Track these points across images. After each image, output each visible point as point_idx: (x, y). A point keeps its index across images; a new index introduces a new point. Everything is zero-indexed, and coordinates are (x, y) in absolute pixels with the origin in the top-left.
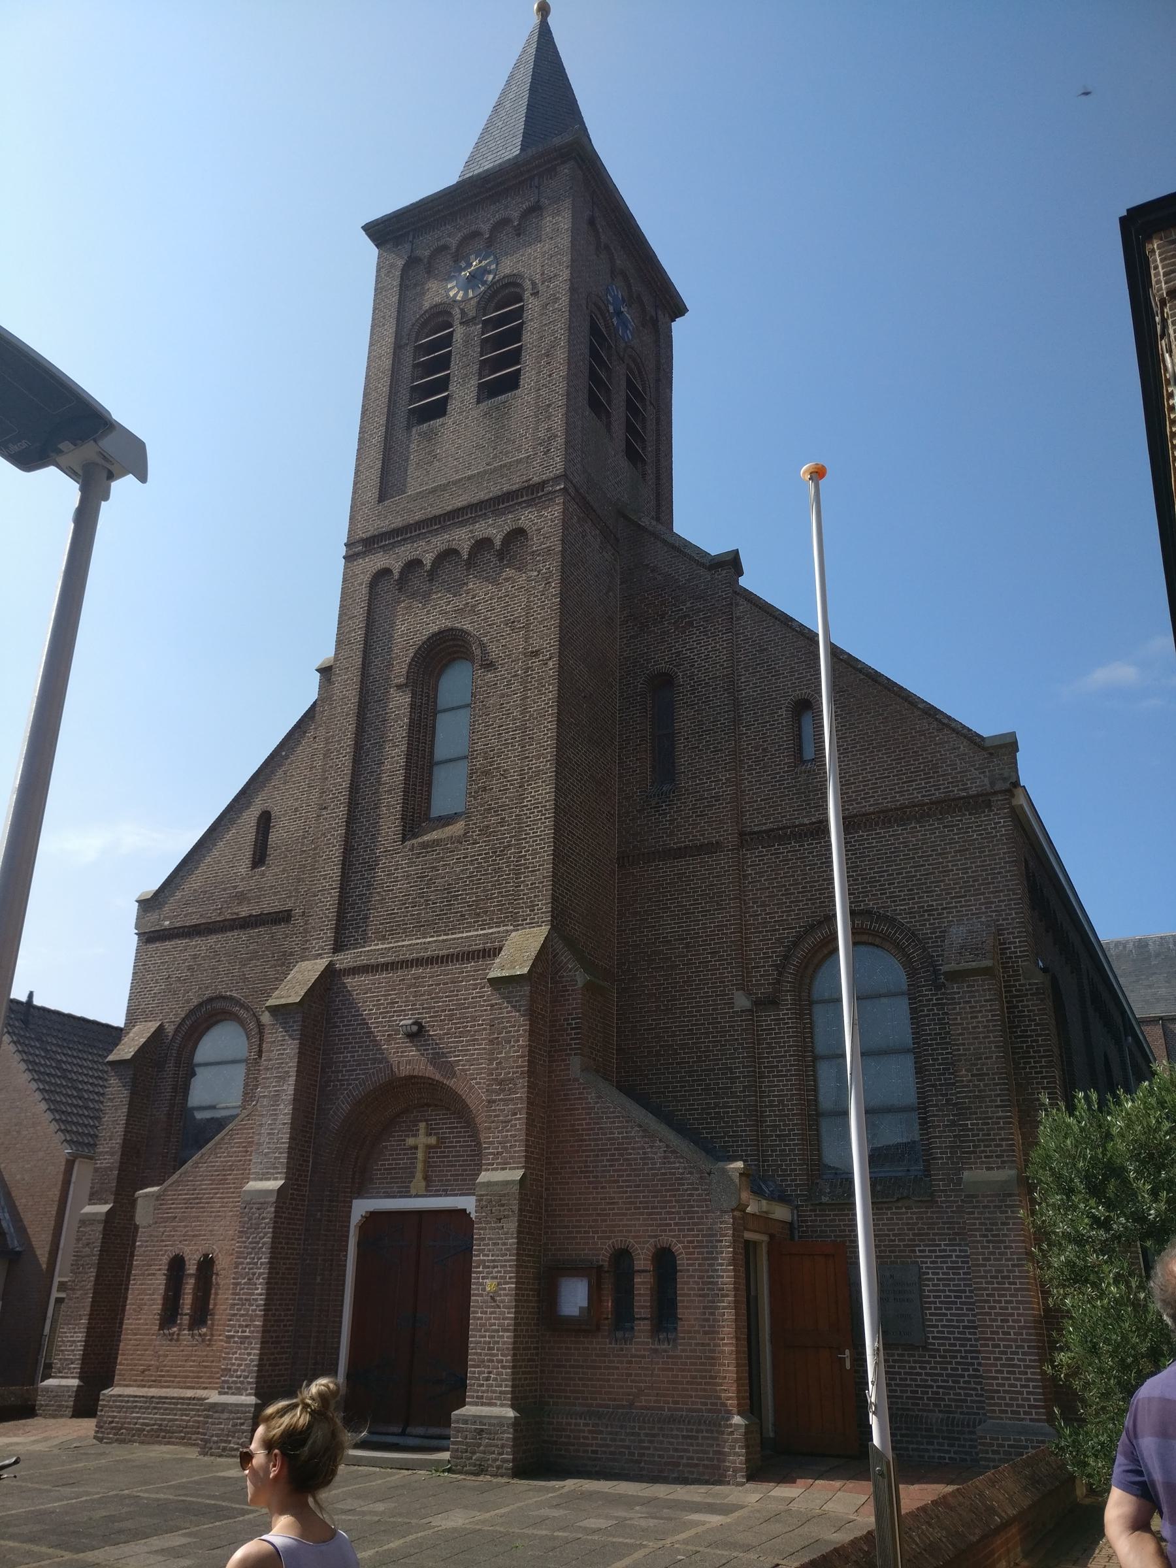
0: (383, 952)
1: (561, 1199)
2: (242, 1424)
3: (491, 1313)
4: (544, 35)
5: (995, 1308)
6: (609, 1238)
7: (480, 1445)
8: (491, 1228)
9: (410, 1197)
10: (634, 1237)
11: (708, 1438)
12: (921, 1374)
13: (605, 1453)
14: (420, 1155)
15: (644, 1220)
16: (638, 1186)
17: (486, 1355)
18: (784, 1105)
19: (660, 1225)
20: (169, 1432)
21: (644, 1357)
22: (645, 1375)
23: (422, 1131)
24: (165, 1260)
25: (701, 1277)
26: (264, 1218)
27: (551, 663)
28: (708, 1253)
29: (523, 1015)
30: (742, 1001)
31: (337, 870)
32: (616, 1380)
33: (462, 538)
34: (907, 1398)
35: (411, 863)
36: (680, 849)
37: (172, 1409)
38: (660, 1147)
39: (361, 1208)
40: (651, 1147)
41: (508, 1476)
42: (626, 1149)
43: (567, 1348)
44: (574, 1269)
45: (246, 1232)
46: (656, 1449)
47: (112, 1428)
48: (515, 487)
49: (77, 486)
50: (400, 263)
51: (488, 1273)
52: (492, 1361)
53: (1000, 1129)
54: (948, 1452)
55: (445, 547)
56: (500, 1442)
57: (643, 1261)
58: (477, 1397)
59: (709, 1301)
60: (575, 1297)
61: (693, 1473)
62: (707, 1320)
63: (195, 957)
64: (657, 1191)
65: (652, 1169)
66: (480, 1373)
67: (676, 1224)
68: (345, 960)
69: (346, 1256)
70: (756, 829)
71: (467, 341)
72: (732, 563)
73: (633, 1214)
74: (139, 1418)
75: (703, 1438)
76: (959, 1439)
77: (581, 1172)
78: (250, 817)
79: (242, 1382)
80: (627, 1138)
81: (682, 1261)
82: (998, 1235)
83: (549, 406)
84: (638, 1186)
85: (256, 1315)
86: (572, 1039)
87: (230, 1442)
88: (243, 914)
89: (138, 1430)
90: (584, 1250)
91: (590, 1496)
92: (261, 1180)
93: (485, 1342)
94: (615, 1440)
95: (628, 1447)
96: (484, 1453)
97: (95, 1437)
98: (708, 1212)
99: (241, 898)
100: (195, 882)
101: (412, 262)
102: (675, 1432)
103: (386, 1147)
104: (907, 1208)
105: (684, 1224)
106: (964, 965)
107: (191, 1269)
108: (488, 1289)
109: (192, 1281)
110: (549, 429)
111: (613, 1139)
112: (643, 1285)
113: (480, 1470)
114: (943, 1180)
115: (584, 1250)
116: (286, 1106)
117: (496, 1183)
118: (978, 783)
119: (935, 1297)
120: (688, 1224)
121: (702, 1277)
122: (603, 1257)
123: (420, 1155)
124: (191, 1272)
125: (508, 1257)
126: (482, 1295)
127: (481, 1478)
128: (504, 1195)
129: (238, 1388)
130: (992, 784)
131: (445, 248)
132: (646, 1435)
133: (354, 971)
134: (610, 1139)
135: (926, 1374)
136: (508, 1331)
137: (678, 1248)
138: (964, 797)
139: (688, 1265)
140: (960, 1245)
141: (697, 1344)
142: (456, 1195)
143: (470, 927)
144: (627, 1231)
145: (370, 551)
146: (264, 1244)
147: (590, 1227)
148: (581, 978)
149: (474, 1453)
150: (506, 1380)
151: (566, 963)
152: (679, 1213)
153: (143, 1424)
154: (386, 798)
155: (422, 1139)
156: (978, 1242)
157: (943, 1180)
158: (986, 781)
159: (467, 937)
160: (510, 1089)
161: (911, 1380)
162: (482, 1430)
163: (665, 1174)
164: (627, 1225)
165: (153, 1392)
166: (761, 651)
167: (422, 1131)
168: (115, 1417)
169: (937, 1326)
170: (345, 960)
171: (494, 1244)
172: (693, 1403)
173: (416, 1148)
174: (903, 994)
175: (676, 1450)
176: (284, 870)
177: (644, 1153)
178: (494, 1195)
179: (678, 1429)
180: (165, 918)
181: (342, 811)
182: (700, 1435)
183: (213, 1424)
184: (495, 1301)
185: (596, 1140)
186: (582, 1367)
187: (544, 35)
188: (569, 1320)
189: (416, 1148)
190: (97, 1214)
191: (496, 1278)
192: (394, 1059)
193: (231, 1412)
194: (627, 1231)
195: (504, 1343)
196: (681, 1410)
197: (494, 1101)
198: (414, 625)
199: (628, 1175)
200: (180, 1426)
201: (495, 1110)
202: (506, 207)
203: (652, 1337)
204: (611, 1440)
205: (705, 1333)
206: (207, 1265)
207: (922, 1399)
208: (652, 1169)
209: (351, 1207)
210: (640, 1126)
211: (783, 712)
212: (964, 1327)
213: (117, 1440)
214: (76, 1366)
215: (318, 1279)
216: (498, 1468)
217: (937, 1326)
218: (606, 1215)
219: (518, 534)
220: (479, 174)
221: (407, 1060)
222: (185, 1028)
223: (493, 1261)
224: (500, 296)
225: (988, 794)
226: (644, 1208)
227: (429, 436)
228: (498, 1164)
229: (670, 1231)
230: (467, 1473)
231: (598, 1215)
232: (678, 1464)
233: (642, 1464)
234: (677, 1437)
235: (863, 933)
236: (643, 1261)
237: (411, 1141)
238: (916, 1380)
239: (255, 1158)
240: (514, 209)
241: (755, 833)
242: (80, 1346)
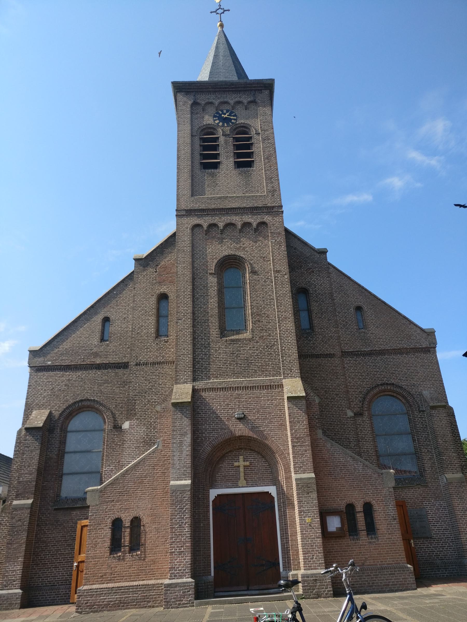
0: (220, 383)
1: (321, 485)
2: (189, 591)
3: (310, 531)
5: (463, 521)
6: (344, 500)
7: (316, 586)
8: (304, 497)
9: (240, 487)
10: (355, 499)
11: (399, 573)
12: (430, 547)
13: (357, 584)
14: (242, 469)
15: (358, 492)
16: (354, 479)
17: (310, 549)
18: (369, 452)
19: (365, 494)
20: (126, 603)
21: (365, 545)
22: (367, 552)
24: (109, 521)
25: (385, 513)
26: (184, 497)
27: (286, 277)
28: (385, 503)
29: (304, 412)
30: (350, 414)
31: (190, 347)
32: (355, 555)
33: (238, 220)
34: (427, 556)
35: (226, 347)
36: (318, 354)
37: (128, 592)
38: (360, 465)
39: (213, 493)
40: (357, 464)
41: (331, 597)
42: (346, 465)
43: (332, 544)
44: (334, 513)
45: (175, 504)
46: (378, 580)
47: (88, 606)
48: (260, 206)
50: (190, 102)
51: (306, 515)
52: (314, 551)
53: (454, 460)
54: (445, 573)
55: (229, 221)
56: (325, 584)
57: (359, 508)
58: (309, 567)
59: (389, 522)
60: (334, 523)
61: (395, 587)
62: (389, 529)
63: (69, 380)
64: (362, 481)
65: (358, 473)
66: (308, 556)
67: (371, 493)
68: (200, 385)
69: (209, 514)
70: (347, 350)
71: (226, 142)
72: (323, 252)
73: (353, 490)
74: (106, 599)
75: (397, 574)
76: (448, 568)
77: (328, 475)
78: (99, 318)
79: (183, 573)
80: (346, 461)
81: (376, 507)
82: (461, 496)
83: (272, 178)
84: (354, 479)
85: (186, 541)
86: (317, 423)
87: (182, 601)
88: (98, 362)
89: (106, 604)
90: (334, 505)
91: (386, 598)
92: (177, 480)
93: (309, 544)
94: (361, 579)
95: (367, 581)
96: (319, 589)
97: (76, 612)
98: (384, 488)
99: (96, 355)
100: (66, 345)
101: (195, 104)
102: (385, 573)
103: (222, 467)
104: (419, 488)
105: (374, 493)
106: (435, 404)
108: (307, 521)
109: (362, 514)
110: (273, 187)
111: (340, 461)
112: (360, 518)
113: (318, 596)
114: (429, 478)
115: (334, 505)
116: (187, 447)
117: (305, 479)
118: (425, 344)
119: (432, 519)
120: (376, 493)
121: (385, 513)
122: (343, 507)
123: (242, 469)
124: (127, 526)
125: (314, 508)
126: (305, 524)
127: (319, 599)
128: (309, 483)
129: (181, 576)
130: (430, 344)
131: (211, 103)
132: (374, 575)
133: (205, 390)
134: (339, 462)
135: (433, 547)
136: (319, 538)
137: (373, 502)
138: (420, 348)
139: (378, 508)
140: (438, 501)
141: (386, 538)
142: (263, 486)
143: (260, 376)
144: (351, 497)
145: (187, 215)
146: (186, 509)
147: (335, 496)
148: (317, 400)
149: (314, 589)
150: (321, 558)
151: (310, 393)
152: (372, 489)
153: (108, 602)
154: (211, 319)
155: (241, 463)
156: (455, 498)
157: (429, 478)
158: (428, 343)
159: (261, 380)
160: (302, 441)
161: (428, 550)
162: (316, 580)
163: (364, 474)
164: (351, 495)
165: (110, 585)
166: (341, 286)
168: (89, 600)
169: (434, 530)
170: (200, 385)
171: (308, 503)
172: (389, 561)
173: (239, 467)
175: (387, 580)
176: (120, 345)
177: (354, 467)
178: (305, 483)
179: (386, 572)
180: (49, 361)
181: (189, 322)
182: (396, 573)
183: (171, 593)
184: (311, 526)
185: (333, 462)
186: (340, 551)
188: (332, 533)
189: (239, 467)
190: (25, 504)
191: (310, 517)
192: (232, 428)
193: (181, 587)
194: (351, 497)
195: (318, 543)
196: (384, 564)
197: (296, 446)
198: (216, 251)
199: (349, 475)
200: (133, 599)
201: (296, 450)
202: (240, 97)
203: (368, 537)
204: (359, 579)
205: (389, 534)
207: (432, 556)
208: (358, 473)
209: (209, 493)
210: (351, 457)
211: (352, 309)
212: (444, 529)
213: (92, 612)
214: (18, 583)
215: (202, 525)
216: (326, 594)
217: (434, 530)
218: (342, 491)
219: (263, 224)
220: (230, 81)
221: (240, 429)
222: (65, 414)
223: (308, 510)
224: (238, 130)
225: (429, 348)
226: (357, 488)
227: (213, 175)
228: (301, 471)
229: (369, 496)
230: (312, 598)
231: (338, 491)
232: (389, 585)
233: (374, 587)
234: (387, 574)
235: (390, 391)
236: (359, 508)
237: (236, 464)
238: (429, 550)
239: (171, 470)
240: (245, 99)
241: (347, 352)
242: (19, 573)
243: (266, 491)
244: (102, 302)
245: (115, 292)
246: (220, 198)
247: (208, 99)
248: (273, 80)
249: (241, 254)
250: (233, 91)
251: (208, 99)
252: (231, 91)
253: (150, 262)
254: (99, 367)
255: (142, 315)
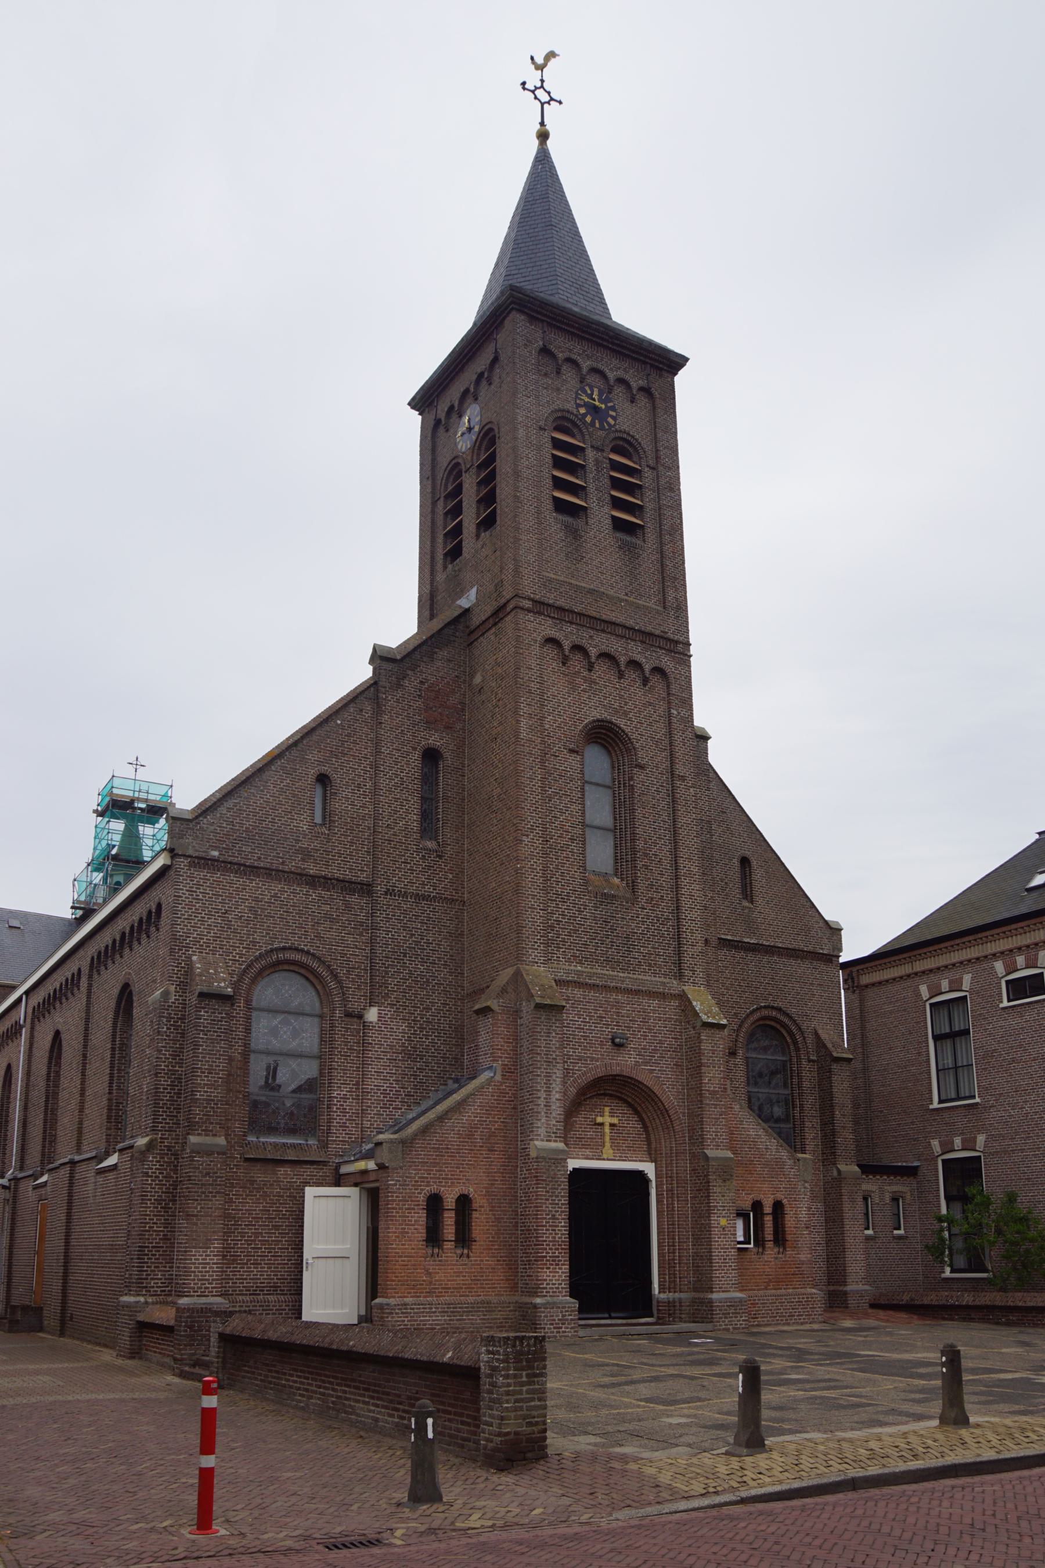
4: (543, 163)
14: (607, 1129)
23: (607, 1114)
24: (422, 1198)
35: (596, 907)
49: (676, 378)
107: (768, 1209)
109: (452, 1214)
137: (785, 1201)
167: (607, 1114)
174: (254, 1052)
176: (352, 843)
187: (543, 163)
189: (602, 1124)
206: (464, 1202)
211: (735, 861)
243: (641, 1169)
244: (315, 737)
245: (339, 722)
246: (591, 592)
247: (570, 351)
248: (686, 360)
249: (621, 722)
250: (613, 351)
251: (570, 351)
252: (610, 349)
253: (409, 672)
254: (313, 881)
255: (396, 786)
